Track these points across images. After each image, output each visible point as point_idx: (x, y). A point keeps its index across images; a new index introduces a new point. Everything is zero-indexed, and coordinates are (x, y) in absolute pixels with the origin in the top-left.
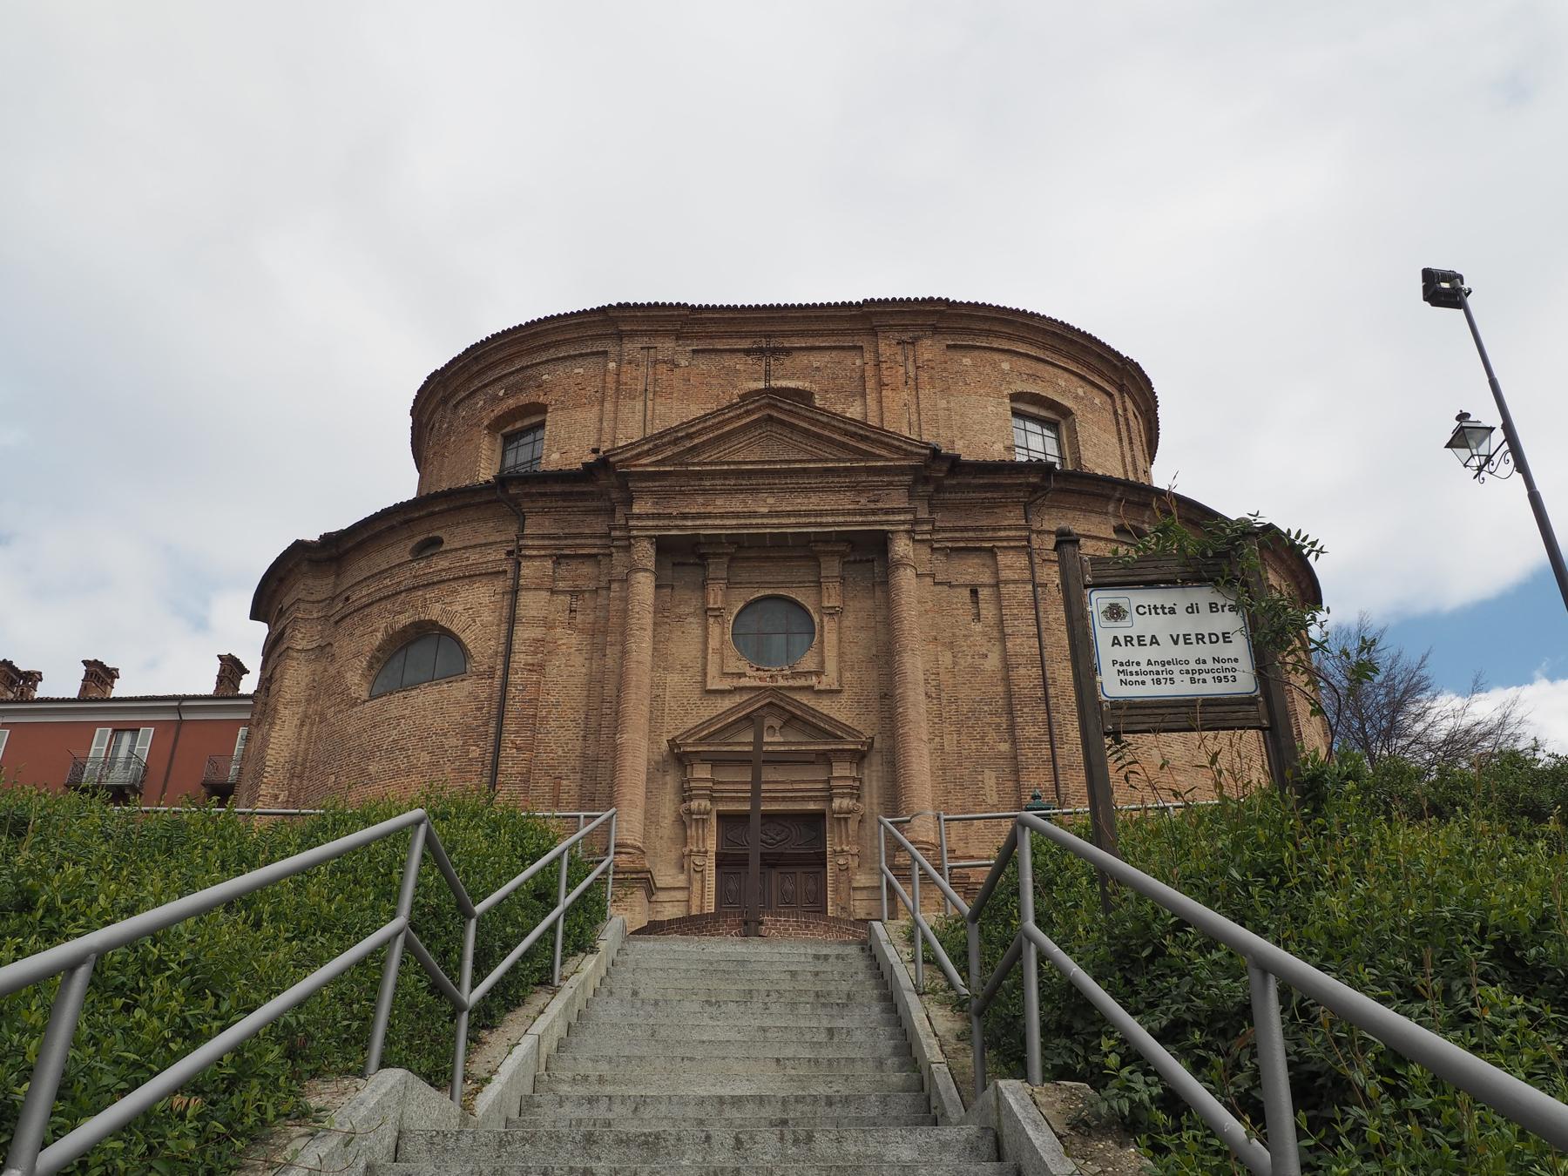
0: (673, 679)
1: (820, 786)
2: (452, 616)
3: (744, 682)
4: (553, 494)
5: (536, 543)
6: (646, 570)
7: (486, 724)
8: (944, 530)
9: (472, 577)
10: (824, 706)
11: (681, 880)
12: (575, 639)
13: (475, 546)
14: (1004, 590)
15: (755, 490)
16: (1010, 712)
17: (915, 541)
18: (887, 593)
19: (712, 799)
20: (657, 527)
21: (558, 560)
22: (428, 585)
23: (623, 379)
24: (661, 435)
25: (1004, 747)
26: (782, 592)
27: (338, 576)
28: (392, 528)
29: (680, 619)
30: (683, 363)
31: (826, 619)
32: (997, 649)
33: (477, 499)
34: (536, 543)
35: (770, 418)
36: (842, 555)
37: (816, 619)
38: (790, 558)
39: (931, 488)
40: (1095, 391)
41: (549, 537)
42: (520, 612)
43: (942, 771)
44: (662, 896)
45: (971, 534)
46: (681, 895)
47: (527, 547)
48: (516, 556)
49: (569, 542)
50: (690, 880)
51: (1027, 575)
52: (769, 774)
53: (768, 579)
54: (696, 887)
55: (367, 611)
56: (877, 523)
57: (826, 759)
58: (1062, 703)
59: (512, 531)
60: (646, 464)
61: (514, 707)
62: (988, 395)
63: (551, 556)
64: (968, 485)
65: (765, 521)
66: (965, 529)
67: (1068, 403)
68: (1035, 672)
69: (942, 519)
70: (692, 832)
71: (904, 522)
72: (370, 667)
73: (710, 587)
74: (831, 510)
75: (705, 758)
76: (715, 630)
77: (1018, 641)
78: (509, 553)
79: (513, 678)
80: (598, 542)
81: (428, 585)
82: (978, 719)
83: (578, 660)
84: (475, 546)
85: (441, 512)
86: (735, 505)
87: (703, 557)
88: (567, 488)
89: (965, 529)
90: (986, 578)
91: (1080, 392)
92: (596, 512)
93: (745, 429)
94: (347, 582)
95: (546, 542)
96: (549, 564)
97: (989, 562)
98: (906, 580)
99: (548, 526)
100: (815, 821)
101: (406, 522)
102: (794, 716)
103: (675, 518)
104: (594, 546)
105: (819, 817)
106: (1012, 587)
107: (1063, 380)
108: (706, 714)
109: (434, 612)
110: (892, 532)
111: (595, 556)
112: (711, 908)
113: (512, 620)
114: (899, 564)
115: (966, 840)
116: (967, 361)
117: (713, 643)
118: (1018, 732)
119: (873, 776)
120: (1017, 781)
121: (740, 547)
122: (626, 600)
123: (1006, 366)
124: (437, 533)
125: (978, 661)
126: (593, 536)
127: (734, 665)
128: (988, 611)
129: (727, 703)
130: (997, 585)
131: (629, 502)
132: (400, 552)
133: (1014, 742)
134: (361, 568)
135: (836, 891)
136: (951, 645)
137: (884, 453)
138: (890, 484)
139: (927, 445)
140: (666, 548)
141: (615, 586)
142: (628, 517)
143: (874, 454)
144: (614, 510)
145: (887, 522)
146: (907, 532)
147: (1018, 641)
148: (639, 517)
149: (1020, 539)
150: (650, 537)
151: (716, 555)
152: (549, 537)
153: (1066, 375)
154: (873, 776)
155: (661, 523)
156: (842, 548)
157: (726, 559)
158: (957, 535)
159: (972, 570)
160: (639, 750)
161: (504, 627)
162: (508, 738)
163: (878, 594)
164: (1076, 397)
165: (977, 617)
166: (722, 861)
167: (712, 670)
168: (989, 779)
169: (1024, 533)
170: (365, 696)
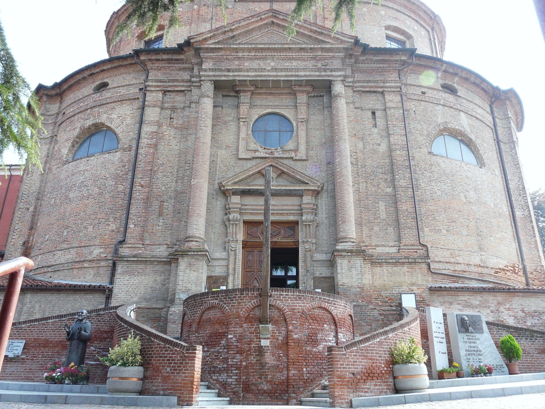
0: (222, 153)
1: (296, 208)
2: (111, 120)
3: (258, 154)
4: (163, 60)
5: (154, 84)
6: (208, 97)
7: (126, 174)
8: (359, 81)
9: (122, 101)
10: (298, 166)
11: (224, 255)
12: (173, 132)
13: (124, 86)
14: (388, 112)
15: (264, 58)
16: (392, 173)
17: (345, 86)
18: (331, 113)
19: (241, 214)
20: (214, 76)
21: (165, 92)
22: (101, 105)
23: (201, 13)
24: (217, 29)
25: (389, 190)
26: (277, 111)
27: (61, 103)
28: (84, 78)
29: (225, 123)
30: (230, 6)
31: (300, 124)
32: (386, 140)
33: (125, 63)
34: (154, 84)
35: (273, 22)
36: (308, 93)
37: (294, 124)
38: (282, 94)
39: (353, 60)
40: (422, 28)
41: (160, 81)
42: (145, 118)
43: (358, 201)
44: (216, 263)
45: (372, 84)
46: (224, 263)
47: (149, 86)
48: (144, 90)
49: (170, 84)
50: (228, 255)
51: (400, 105)
52: (273, 201)
53: (270, 104)
54: (232, 259)
55: (72, 119)
56: (324, 75)
57: (299, 194)
58: (417, 169)
59: (144, 77)
60: (210, 44)
61: (141, 165)
62: (374, 25)
63: (161, 91)
64: (371, 60)
65: (269, 73)
66: (369, 81)
67: (411, 32)
68: (404, 153)
69: (358, 76)
70: (230, 230)
71: (340, 76)
72: (73, 146)
73: (241, 107)
74: (304, 69)
75: (235, 193)
76: (243, 129)
77: (396, 138)
78: (140, 89)
79: (140, 151)
80: (185, 84)
81: (101, 105)
82: (376, 176)
83: (174, 142)
84: (124, 86)
85: (108, 70)
86: (255, 64)
87: (238, 92)
88: (170, 57)
89: (369, 81)
90: (379, 106)
91: (416, 28)
92: (184, 69)
93: (260, 28)
94: (64, 105)
95: (159, 84)
96: (160, 95)
97: (380, 98)
98: (342, 106)
99: (160, 75)
100: (293, 226)
101: (92, 75)
102: (283, 172)
103: (224, 71)
104: (183, 86)
105: (297, 223)
106: (392, 111)
107: (409, 21)
108: (238, 170)
109: (103, 119)
110: (334, 81)
111: (183, 91)
112: (239, 284)
113: (141, 122)
114: (337, 96)
115: (370, 237)
116: (365, 9)
117: (243, 135)
118: (396, 183)
119: (323, 202)
120: (396, 207)
121: (257, 87)
122: (197, 112)
123: (383, 13)
124: (106, 80)
125: (375, 147)
126: (183, 81)
127: (252, 146)
128: (380, 122)
129: (249, 164)
130: (385, 110)
131: (200, 64)
132: (88, 89)
133: (394, 187)
134: (70, 98)
135: (305, 261)
136: (362, 139)
137: (330, 41)
138: (333, 57)
139: (351, 37)
140: (218, 86)
141: (193, 105)
142: (200, 70)
143: (325, 42)
144: (193, 69)
145: (332, 76)
146: (342, 81)
147: (396, 138)
148: (205, 70)
149: (397, 87)
150: (211, 81)
151: (244, 91)
152: (160, 81)
153: (410, 19)
154: (323, 202)
155: (216, 74)
156: (308, 88)
157: (249, 94)
158: (366, 84)
159: (372, 102)
160: (203, 187)
161: (138, 125)
162: (137, 180)
163: (326, 112)
164: (414, 30)
165: (375, 126)
166: (245, 245)
167: (241, 149)
168: (382, 206)
169: (398, 85)
170: (71, 159)
